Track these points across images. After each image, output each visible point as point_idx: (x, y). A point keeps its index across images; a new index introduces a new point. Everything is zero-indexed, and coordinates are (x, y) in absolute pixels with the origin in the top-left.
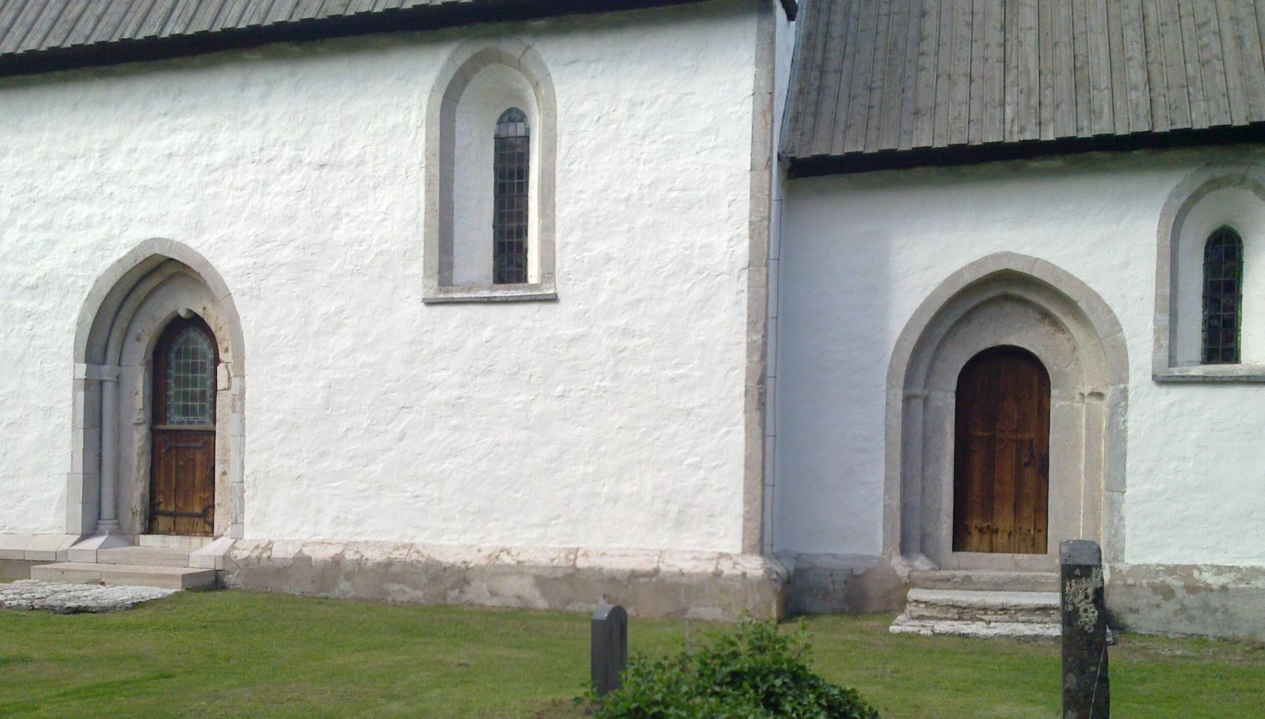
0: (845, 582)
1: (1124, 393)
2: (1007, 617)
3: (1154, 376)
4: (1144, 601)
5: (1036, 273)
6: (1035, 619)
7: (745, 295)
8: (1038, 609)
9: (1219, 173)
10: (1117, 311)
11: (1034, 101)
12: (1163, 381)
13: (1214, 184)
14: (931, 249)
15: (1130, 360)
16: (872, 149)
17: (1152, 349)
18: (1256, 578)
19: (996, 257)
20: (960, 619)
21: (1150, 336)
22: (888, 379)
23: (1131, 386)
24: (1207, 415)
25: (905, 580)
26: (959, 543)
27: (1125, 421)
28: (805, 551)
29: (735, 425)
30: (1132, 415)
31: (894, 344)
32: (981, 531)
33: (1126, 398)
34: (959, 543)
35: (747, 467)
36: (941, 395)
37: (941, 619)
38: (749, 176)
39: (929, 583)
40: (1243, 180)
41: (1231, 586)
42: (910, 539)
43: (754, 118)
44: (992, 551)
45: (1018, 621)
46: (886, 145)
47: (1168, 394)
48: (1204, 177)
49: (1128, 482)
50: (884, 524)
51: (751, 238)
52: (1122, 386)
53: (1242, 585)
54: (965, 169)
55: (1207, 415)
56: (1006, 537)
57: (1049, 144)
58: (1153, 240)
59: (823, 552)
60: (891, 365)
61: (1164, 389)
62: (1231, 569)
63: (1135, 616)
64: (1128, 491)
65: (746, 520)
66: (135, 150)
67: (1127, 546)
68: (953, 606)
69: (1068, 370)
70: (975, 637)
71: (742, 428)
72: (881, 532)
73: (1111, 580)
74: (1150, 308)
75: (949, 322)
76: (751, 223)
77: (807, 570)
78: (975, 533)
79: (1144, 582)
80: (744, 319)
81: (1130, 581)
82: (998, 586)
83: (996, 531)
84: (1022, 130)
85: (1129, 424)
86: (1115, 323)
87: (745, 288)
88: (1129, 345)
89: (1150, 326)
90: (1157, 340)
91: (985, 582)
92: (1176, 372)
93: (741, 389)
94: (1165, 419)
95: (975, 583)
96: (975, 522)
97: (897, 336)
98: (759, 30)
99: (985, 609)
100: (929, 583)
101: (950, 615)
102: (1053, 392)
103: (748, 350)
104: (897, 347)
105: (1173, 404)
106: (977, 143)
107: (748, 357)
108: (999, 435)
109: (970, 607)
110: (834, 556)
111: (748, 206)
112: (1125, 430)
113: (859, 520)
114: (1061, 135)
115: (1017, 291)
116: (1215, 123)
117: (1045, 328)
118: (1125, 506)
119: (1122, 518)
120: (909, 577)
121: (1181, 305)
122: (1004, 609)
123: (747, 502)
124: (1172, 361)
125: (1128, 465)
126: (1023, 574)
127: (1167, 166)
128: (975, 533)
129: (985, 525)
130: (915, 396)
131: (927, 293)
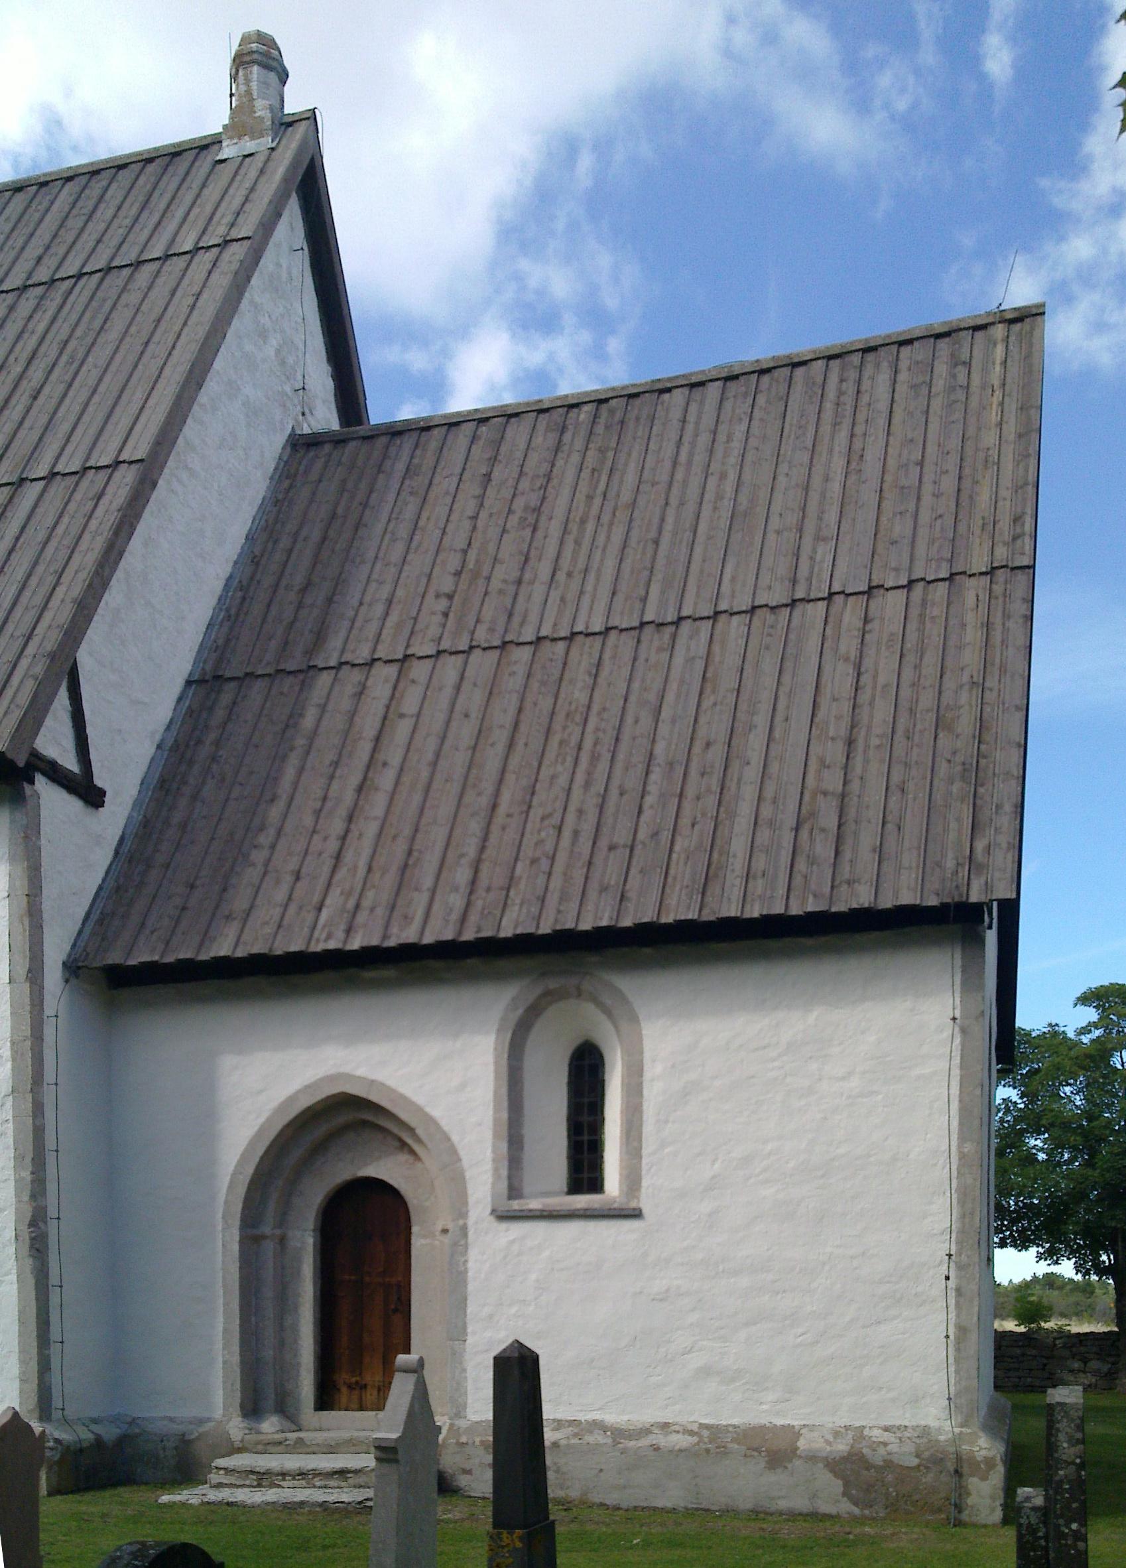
0: (176, 1448)
1: (464, 1230)
2: (304, 1482)
3: (493, 1211)
4: (477, 1461)
5: (374, 1097)
6: (332, 1483)
7: (10, 1125)
8: (336, 1473)
9: (553, 984)
10: (455, 1138)
11: (351, 904)
12: (505, 1217)
13: (549, 998)
14: (261, 1074)
15: (470, 1191)
16: (169, 959)
17: (490, 1180)
18: (591, 1432)
19: (330, 1079)
20: (259, 1485)
21: (488, 1166)
22: (223, 1218)
23: (471, 1220)
24: (546, 1253)
25: (237, 1444)
26: (325, 1400)
27: (466, 1261)
28: (147, 1415)
29: (6, 1274)
30: (473, 1255)
31: (228, 1178)
32: (350, 1387)
33: (465, 1235)
34: (325, 1400)
35: (22, 1322)
36: (298, 1234)
37: (238, 1487)
38: (8, 990)
39: (260, 1447)
40: (579, 994)
41: (563, 1442)
42: (260, 1395)
43: (10, 924)
44: (362, 1410)
45: (314, 1487)
46: (185, 954)
47: (507, 1230)
48: (538, 990)
49: (469, 1330)
50: (224, 1382)
51: (14, 1060)
52: (461, 1222)
53: (575, 1441)
54: (773, 944)
55: (546, 1253)
56: (375, 1392)
57: (467, 944)
58: (489, 1058)
59: (161, 1415)
60: (226, 1202)
61: (504, 1225)
62: (572, 1423)
63: (468, 1477)
64: (470, 1340)
65: (23, 1381)
66: (536, 844)
67: (469, 1401)
68: (252, 1472)
69: (427, 1204)
70: (243, 1506)
71: (13, 1277)
72: (221, 1392)
73: (445, 1440)
74: (488, 1135)
75: (297, 1153)
76: (13, 1043)
77: (137, 1436)
78: (344, 1390)
79: (477, 1440)
80: (11, 1153)
81: (464, 1439)
82: (331, 1449)
83: (365, 1386)
84: (329, 937)
85: (470, 1265)
86: (453, 1151)
87: (10, 1117)
88: (468, 1175)
89: (489, 1154)
90: (496, 1170)
91: (318, 1445)
92: (516, 1205)
93: (10, 1234)
94: (505, 1257)
95: (308, 1446)
96: (343, 1377)
97: (231, 1169)
98: (12, 821)
99: (284, 1475)
100: (260, 1447)
101: (248, 1482)
102: (415, 1229)
103: (16, 1189)
104: (231, 1182)
105: (513, 1241)
106: (279, 952)
107: (17, 1195)
108: (367, 1279)
109: (268, 1473)
110: (171, 1420)
111: (9, 1023)
112: (466, 1271)
113: (198, 1379)
114: (365, 944)
115: (369, 1117)
116: (519, 931)
117: (403, 1157)
118: (467, 1356)
119: (464, 1370)
120: (242, 1441)
121: (531, 1131)
122: (302, 1474)
123: (23, 1362)
124: (514, 1191)
125: (469, 1311)
126: (356, 1434)
127: (500, 977)
128: (344, 1390)
129: (354, 1380)
130: (263, 1237)
131: (262, 1120)
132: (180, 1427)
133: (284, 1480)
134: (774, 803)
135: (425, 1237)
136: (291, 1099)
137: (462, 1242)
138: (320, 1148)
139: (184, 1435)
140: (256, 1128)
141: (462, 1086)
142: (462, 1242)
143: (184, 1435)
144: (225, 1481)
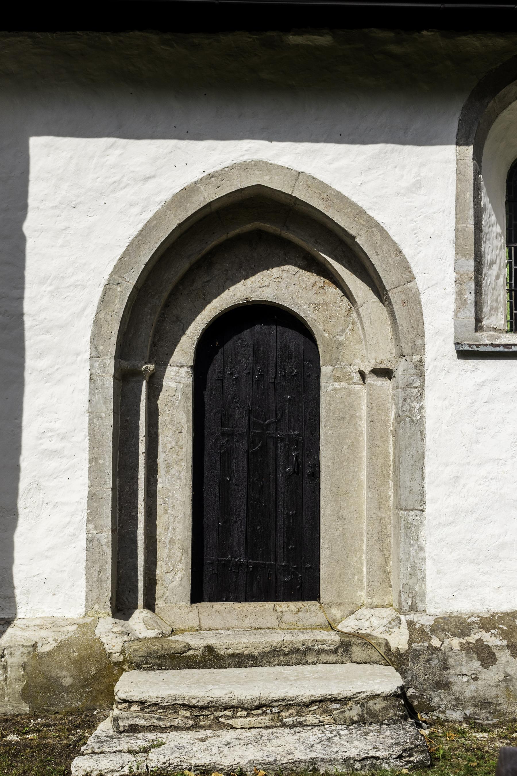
0: (24, 666)
20: (196, 727)
27: (422, 408)
33: (421, 375)
64: (429, 508)
75: (182, 266)
85: (428, 412)
88: (424, 298)
102: (325, 370)
105: (482, 384)
109: (210, 707)
119: (421, 549)
120: (123, 652)
126: (289, 638)
132: (27, 634)
133: (233, 716)
134: (131, 205)
135: (338, 379)
136: (188, 192)
137: (418, 384)
138: (206, 262)
139: (35, 646)
140: (140, 227)
141: (417, 186)
142: (418, 384)
143: (35, 646)
144: (141, 722)
